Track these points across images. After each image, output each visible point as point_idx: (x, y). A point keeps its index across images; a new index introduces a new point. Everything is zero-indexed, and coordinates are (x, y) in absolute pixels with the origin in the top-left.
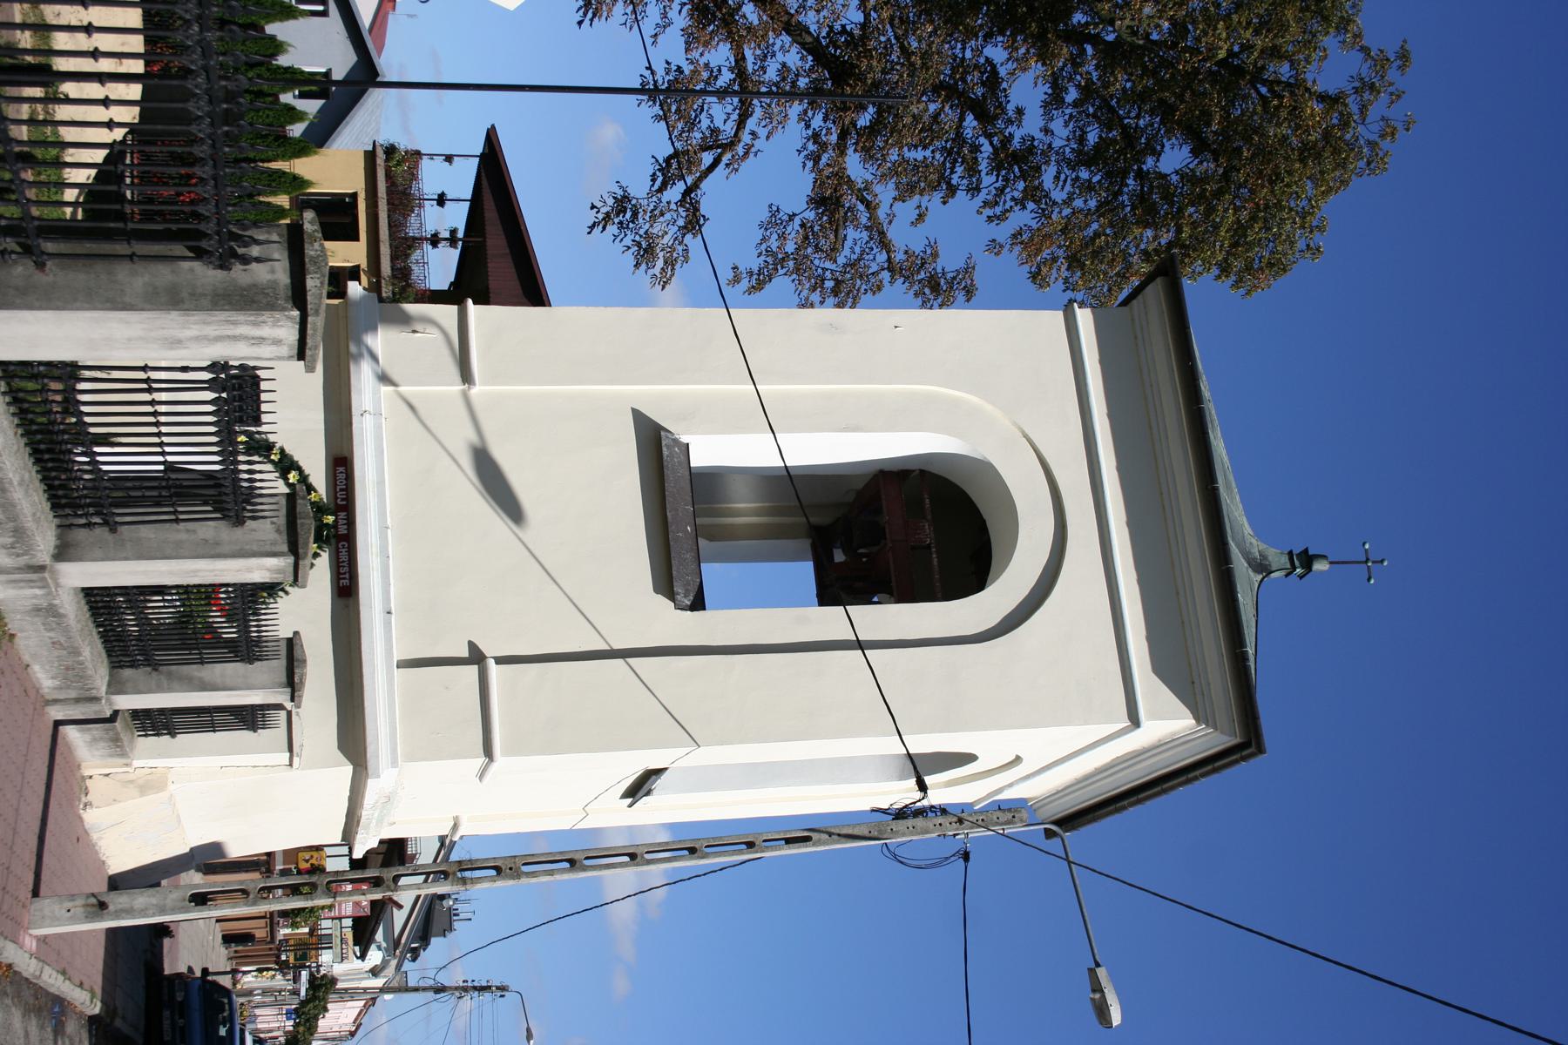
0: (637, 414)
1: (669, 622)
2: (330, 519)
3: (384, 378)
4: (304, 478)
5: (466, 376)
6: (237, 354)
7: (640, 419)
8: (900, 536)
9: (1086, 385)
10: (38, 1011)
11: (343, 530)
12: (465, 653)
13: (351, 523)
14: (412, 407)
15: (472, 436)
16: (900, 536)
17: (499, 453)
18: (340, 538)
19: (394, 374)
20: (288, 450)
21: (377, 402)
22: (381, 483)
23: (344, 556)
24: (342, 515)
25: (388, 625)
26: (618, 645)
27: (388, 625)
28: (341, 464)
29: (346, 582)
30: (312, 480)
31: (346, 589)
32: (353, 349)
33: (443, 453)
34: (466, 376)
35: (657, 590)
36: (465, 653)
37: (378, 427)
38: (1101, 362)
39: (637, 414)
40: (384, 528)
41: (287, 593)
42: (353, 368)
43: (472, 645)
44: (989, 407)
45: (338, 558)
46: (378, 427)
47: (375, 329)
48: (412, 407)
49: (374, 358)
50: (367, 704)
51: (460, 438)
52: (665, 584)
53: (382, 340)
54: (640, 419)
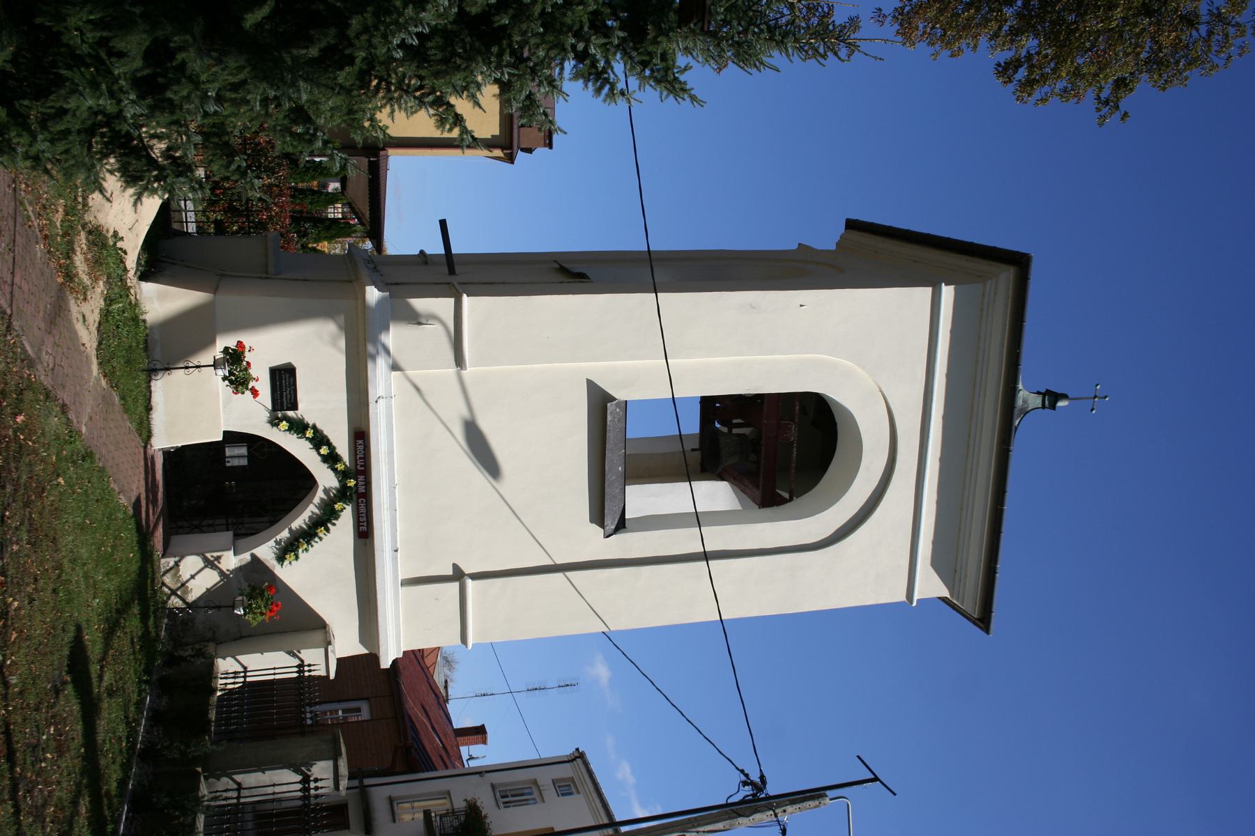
0: (591, 384)
1: (595, 543)
2: (352, 483)
3: (395, 367)
4: (332, 448)
5: (459, 360)
6: (275, 562)
7: (592, 387)
8: (774, 448)
9: (935, 352)
10: (164, 686)
11: (362, 490)
12: (450, 572)
13: (368, 483)
14: (418, 389)
15: (465, 412)
16: (774, 448)
17: (484, 425)
18: (360, 495)
19: (402, 364)
20: (319, 426)
21: (389, 387)
22: (391, 453)
23: (363, 510)
24: (361, 478)
25: (395, 559)
26: (560, 561)
27: (395, 559)
28: (360, 436)
29: (364, 528)
30: (339, 451)
31: (364, 532)
32: (370, 348)
33: (439, 423)
34: (459, 360)
35: (592, 521)
36: (450, 572)
37: (389, 408)
38: (952, 331)
39: (591, 384)
40: (392, 488)
41: (321, 539)
42: (370, 365)
43: (455, 566)
44: (859, 370)
45: (358, 510)
46: (389, 408)
47: (387, 329)
48: (418, 389)
49: (387, 352)
50: (381, 643)
51: (455, 412)
52: (598, 516)
53: (395, 337)
54: (592, 387)
